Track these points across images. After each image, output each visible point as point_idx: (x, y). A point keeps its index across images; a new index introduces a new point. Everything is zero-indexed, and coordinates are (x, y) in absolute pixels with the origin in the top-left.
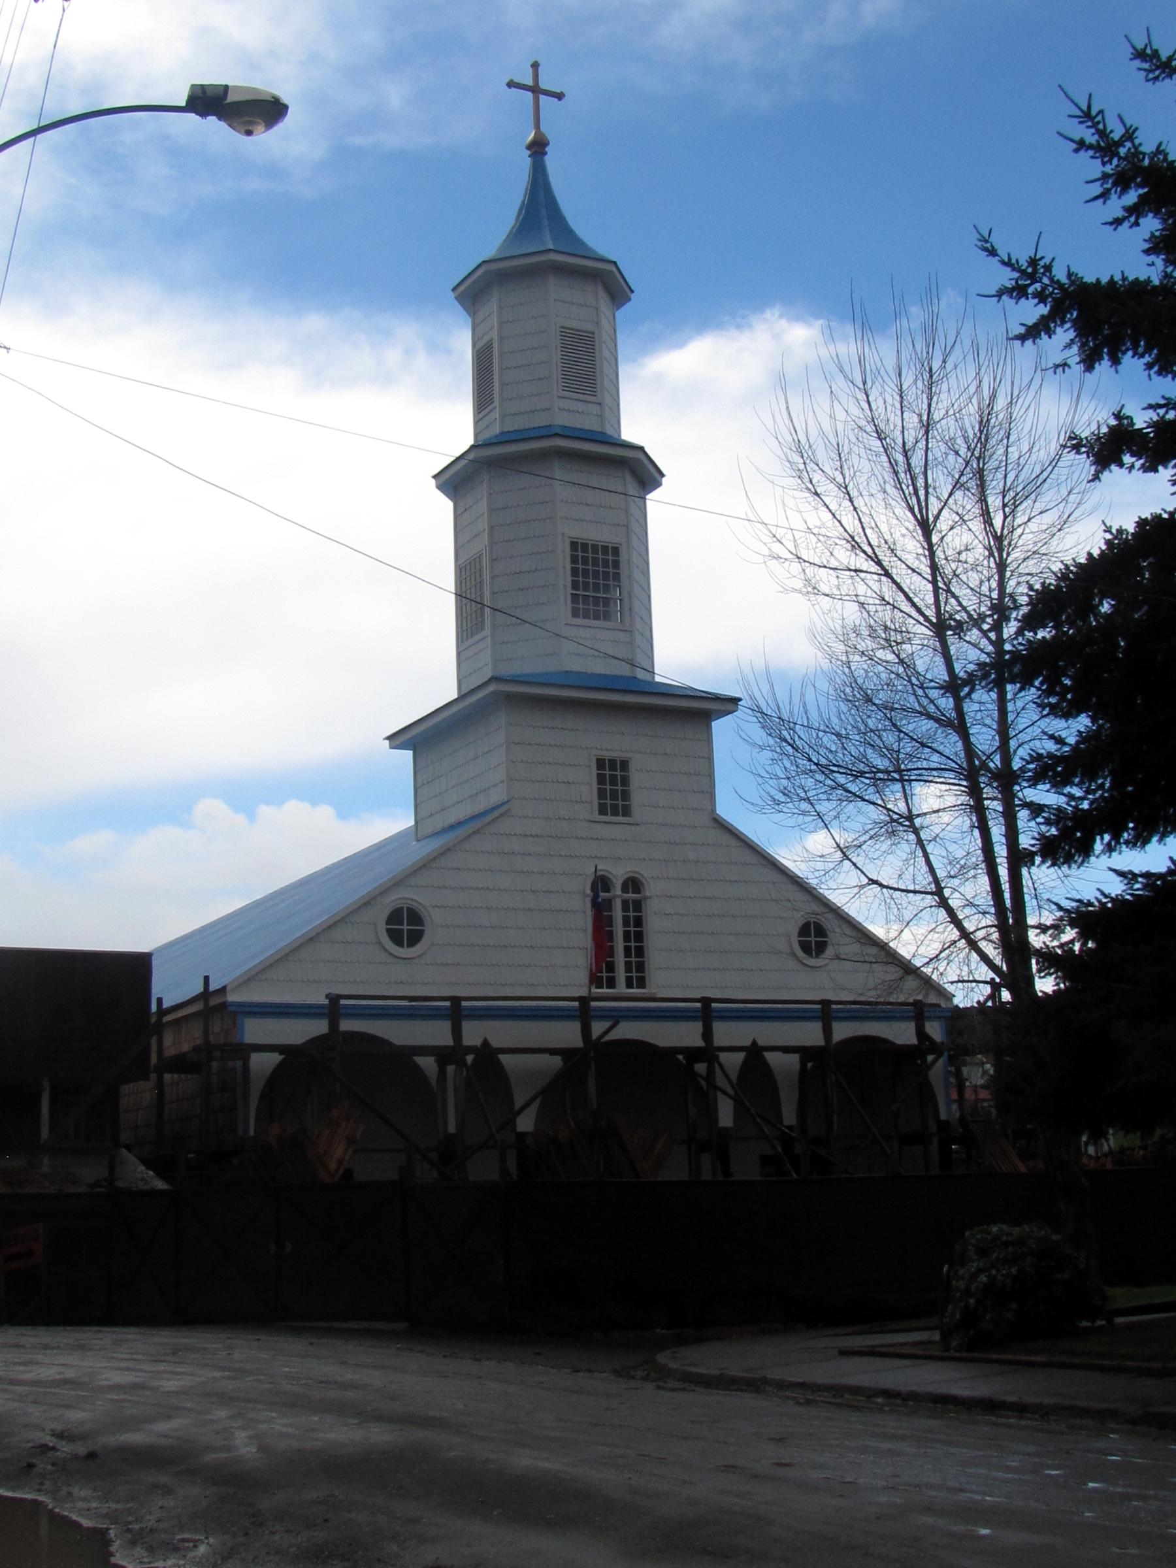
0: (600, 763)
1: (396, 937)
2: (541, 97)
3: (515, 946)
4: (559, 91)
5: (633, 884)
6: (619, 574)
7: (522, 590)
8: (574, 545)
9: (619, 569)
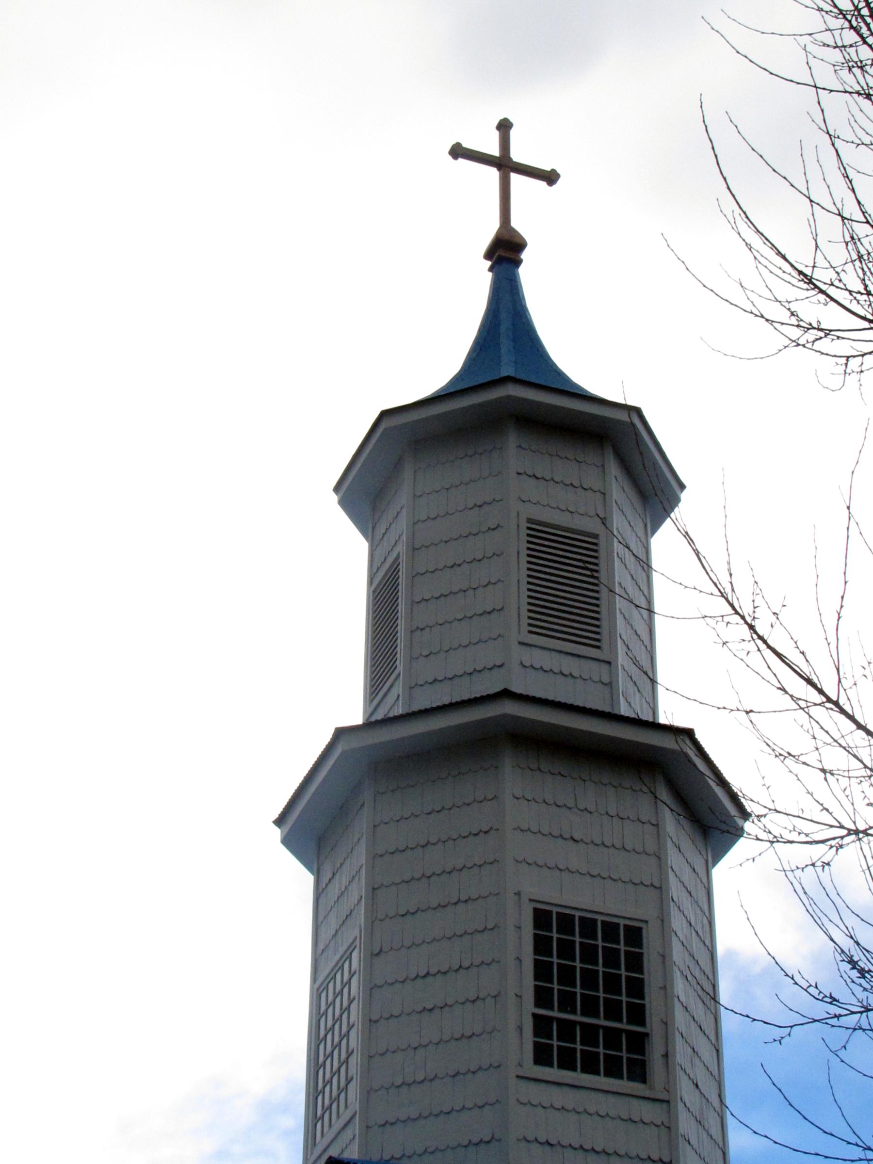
4: (549, 169)
6: (641, 981)
7: (431, 1010)
8: (541, 918)
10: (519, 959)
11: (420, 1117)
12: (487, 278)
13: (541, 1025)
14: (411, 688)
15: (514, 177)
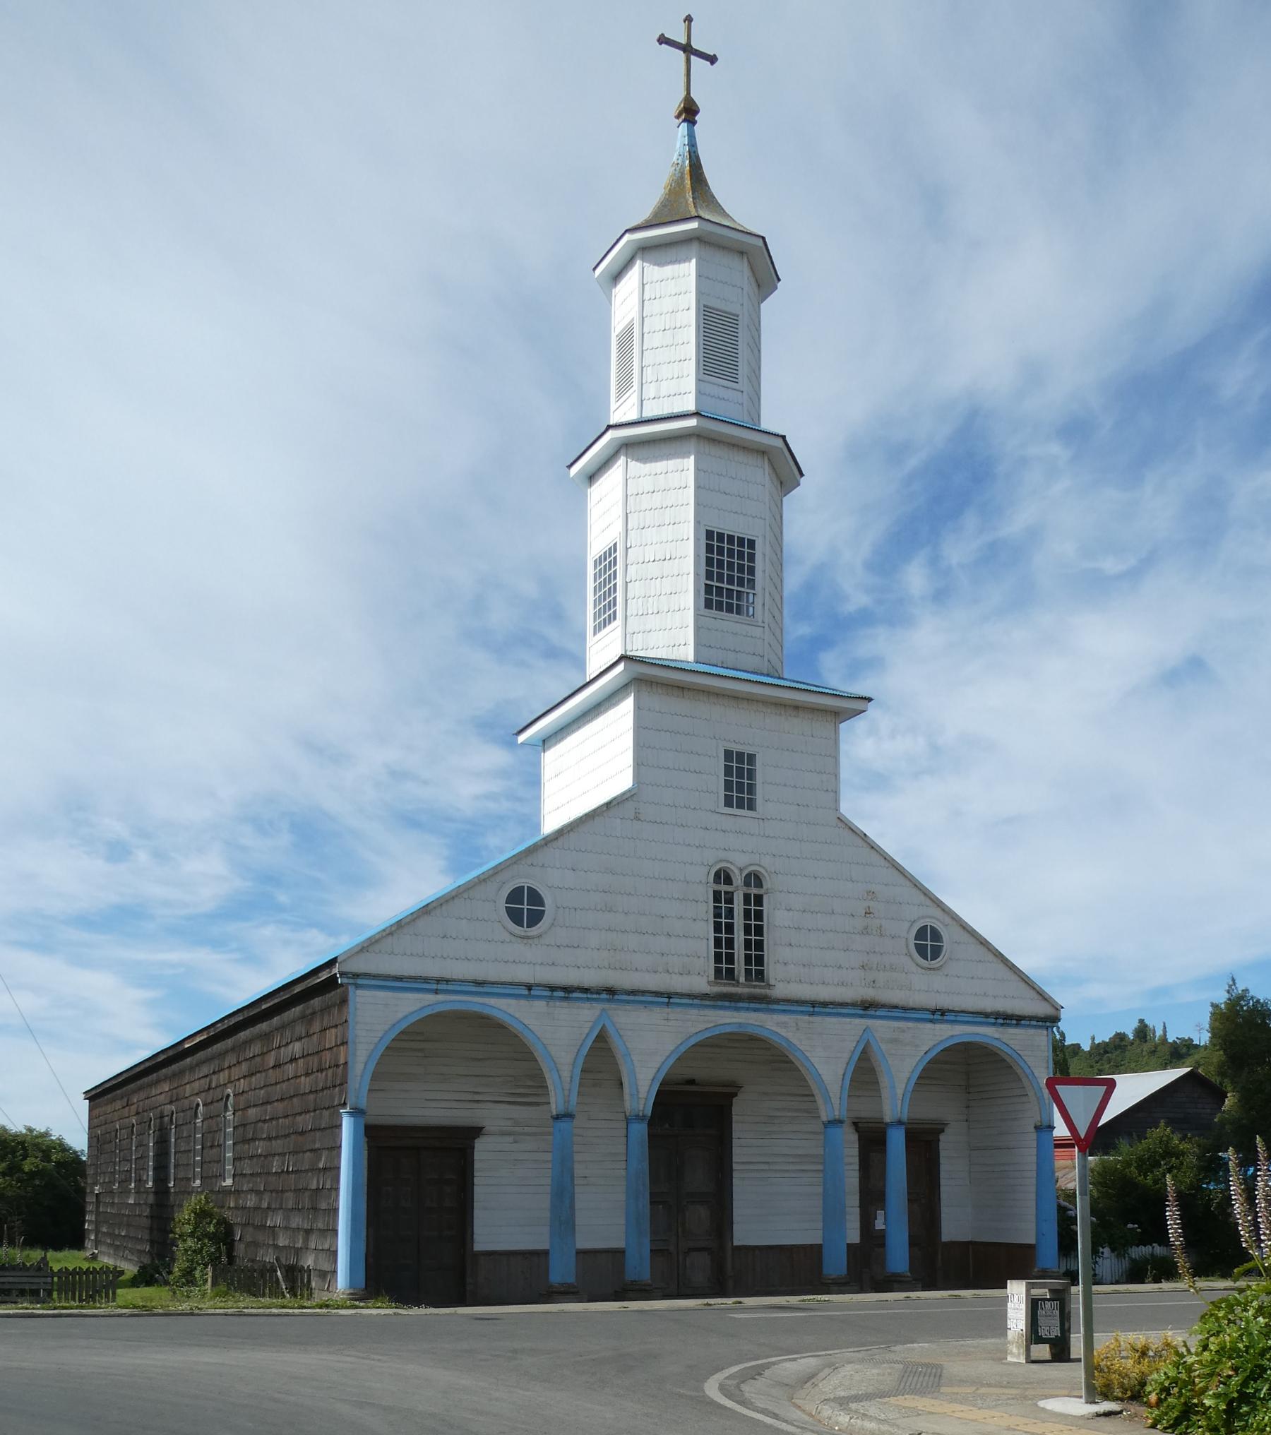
0: (728, 755)
1: (515, 916)
2: (693, 58)
3: (705, 394)
4: (712, 54)
5: (754, 879)
9: (754, 575)
15: (683, 41)
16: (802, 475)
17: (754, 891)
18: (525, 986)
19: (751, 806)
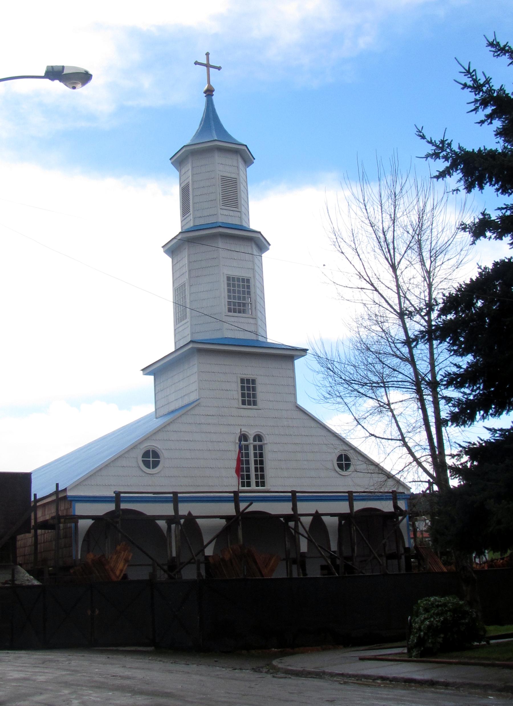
1: (147, 464)
5: (258, 437)
8: (228, 278)
10: (224, 281)
11: (203, 323)
12: (205, 99)
13: (229, 303)
14: (194, 203)
15: (205, 62)
16: (270, 245)
17: (257, 443)
18: (221, 517)
19: (255, 403)
